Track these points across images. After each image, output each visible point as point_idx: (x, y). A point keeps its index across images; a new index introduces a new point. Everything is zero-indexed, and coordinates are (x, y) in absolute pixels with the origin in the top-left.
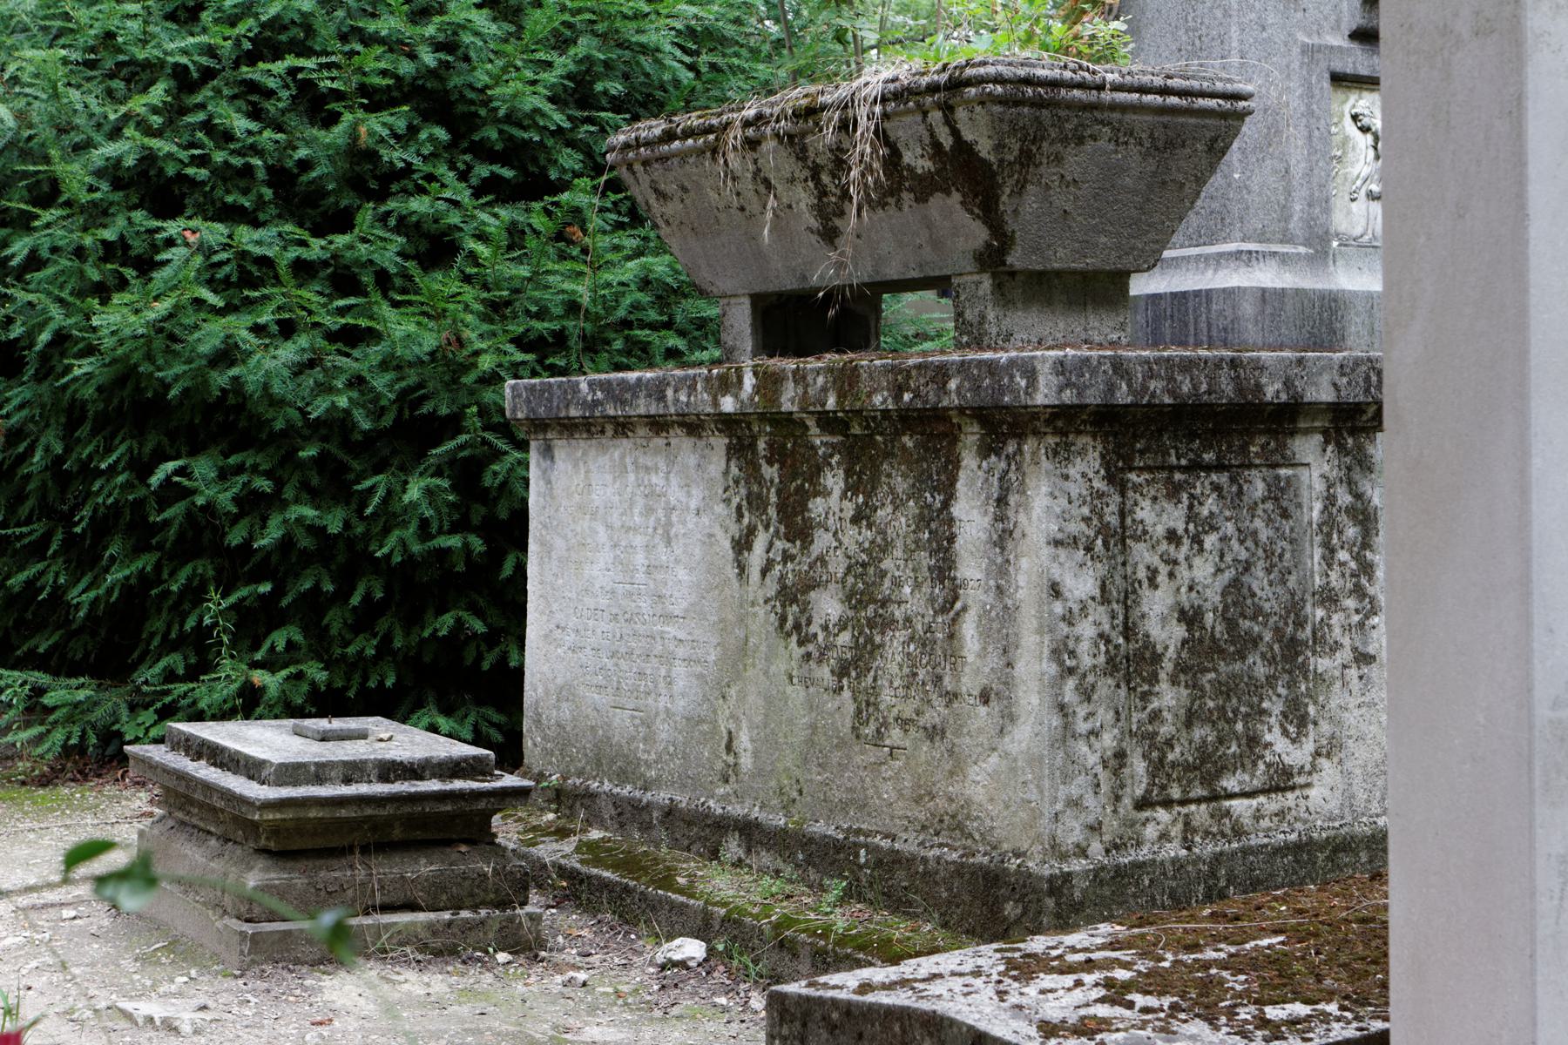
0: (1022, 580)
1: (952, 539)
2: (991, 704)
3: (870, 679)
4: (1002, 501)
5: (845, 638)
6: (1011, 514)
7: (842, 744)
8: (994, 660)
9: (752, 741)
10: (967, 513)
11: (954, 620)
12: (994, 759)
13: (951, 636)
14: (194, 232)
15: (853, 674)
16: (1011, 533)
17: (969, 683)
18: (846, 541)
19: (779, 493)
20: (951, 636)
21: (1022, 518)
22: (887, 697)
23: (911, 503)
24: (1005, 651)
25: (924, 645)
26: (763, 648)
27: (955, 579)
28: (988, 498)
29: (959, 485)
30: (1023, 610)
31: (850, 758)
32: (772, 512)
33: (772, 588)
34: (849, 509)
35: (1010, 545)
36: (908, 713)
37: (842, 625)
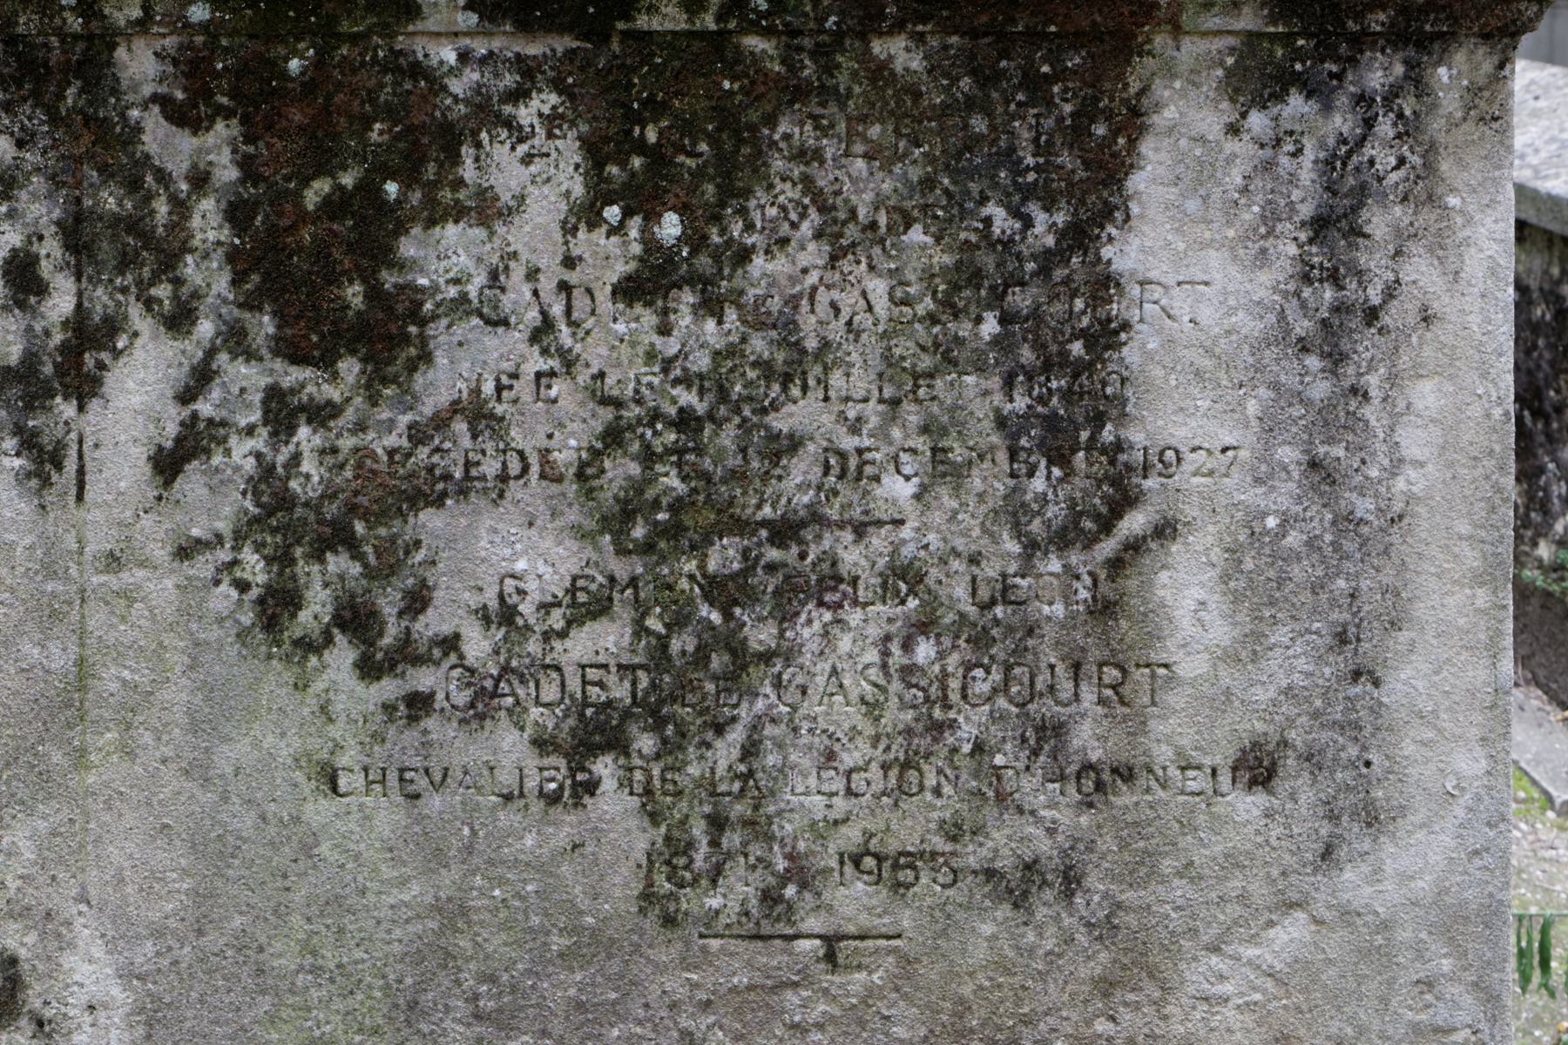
0: (1414, 441)
1: (1106, 336)
2: (1282, 785)
3: (726, 751)
4: (1335, 224)
5: (605, 639)
6: (1374, 261)
7: (591, 945)
8: (1294, 660)
9: (128, 975)
10: (1179, 260)
11: (1116, 565)
12: (1292, 932)
13: (1104, 609)
14: (860, 531)
15: (646, 743)
16: (1372, 315)
17: (1183, 729)
18: (595, 354)
19: (237, 214)
20: (1104, 609)
21: (1420, 271)
22: (806, 797)
23: (916, 235)
24: (1342, 638)
25: (982, 640)
26: (178, 694)
27: (1119, 446)
28: (1271, 218)
29: (1137, 182)
30: (1423, 522)
31: (629, 985)
32: (209, 277)
33: (213, 500)
34: (609, 255)
35: (1366, 345)
36: (911, 828)
37: (586, 605)
